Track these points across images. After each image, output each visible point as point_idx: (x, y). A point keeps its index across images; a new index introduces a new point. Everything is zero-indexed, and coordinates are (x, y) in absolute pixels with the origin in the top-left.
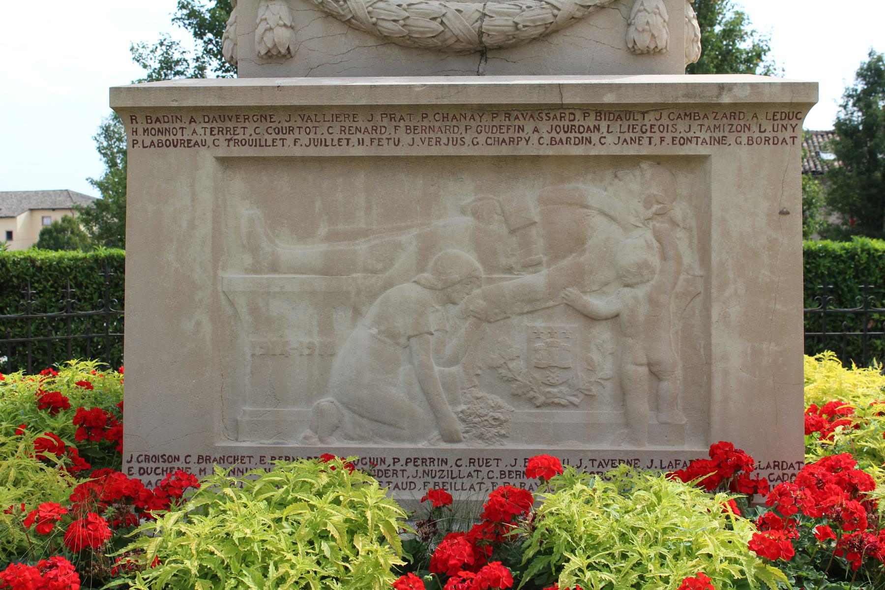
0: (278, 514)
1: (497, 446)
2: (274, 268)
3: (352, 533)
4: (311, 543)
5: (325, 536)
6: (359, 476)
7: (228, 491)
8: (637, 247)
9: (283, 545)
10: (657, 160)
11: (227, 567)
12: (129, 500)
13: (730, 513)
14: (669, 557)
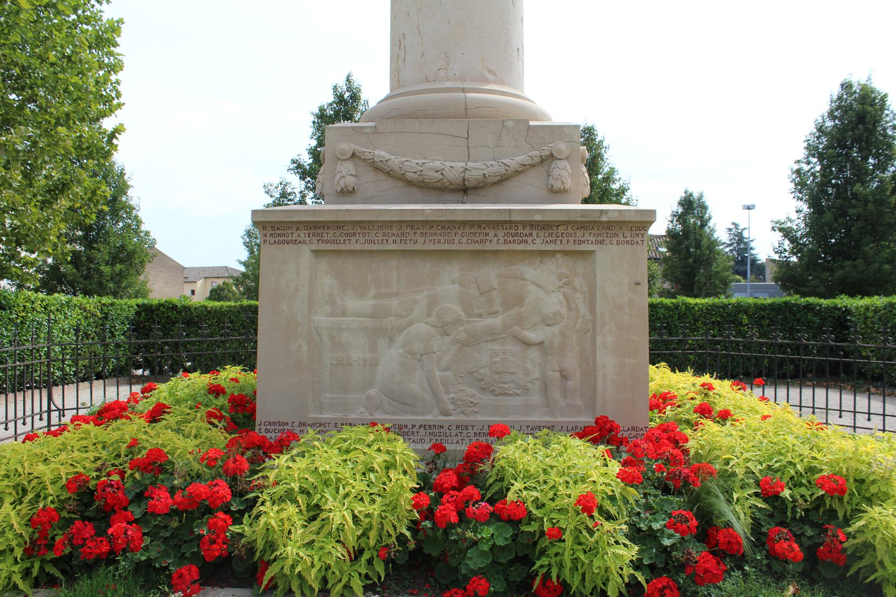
0: (345, 457)
2: (344, 314)
3: (388, 468)
4: (364, 474)
5: (372, 470)
6: (392, 435)
7: (316, 443)
8: (553, 302)
9: (347, 475)
10: (566, 253)
13: (607, 457)
14: (571, 482)
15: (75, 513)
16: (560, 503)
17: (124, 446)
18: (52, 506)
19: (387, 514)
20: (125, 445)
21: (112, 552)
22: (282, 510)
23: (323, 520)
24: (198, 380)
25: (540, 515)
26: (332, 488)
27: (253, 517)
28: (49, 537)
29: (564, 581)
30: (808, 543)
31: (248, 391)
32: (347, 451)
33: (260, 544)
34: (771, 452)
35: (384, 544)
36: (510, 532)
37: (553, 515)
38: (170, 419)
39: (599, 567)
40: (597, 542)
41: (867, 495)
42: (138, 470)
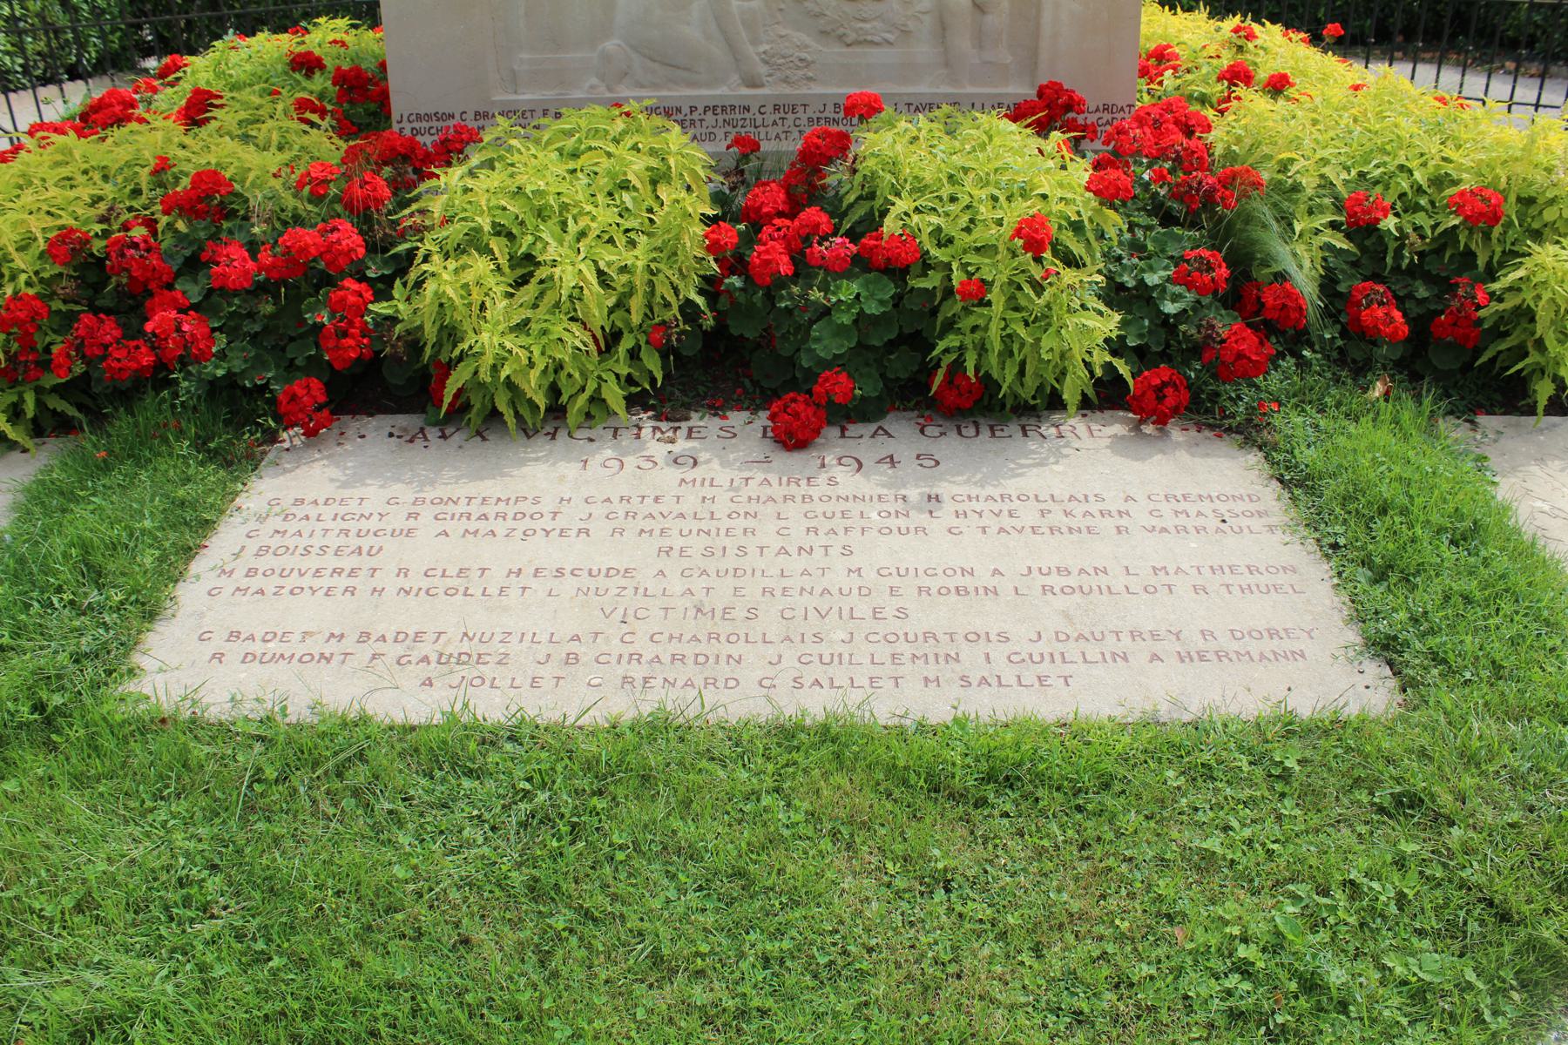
0: (571, 165)
1: (804, 91)
3: (654, 183)
4: (610, 194)
5: (625, 186)
6: (658, 121)
7: (514, 142)
9: (580, 197)
11: (522, 223)
12: (406, 158)
13: (1065, 152)
14: (1002, 199)
15: (77, 303)
16: (980, 236)
17: (144, 175)
18: (31, 292)
19: (661, 266)
20: (147, 170)
21: (161, 366)
22: (464, 267)
23: (542, 282)
24: (268, 45)
25: (945, 259)
26: (553, 223)
27: (410, 285)
28: (40, 347)
29: (988, 375)
30: (1415, 310)
31: (369, 65)
32: (575, 155)
33: (430, 333)
34: (1367, 148)
35: (657, 320)
36: (891, 290)
37: (967, 259)
38: (225, 117)
39: (1051, 349)
40: (1048, 306)
41: (1536, 226)
42: (180, 215)
